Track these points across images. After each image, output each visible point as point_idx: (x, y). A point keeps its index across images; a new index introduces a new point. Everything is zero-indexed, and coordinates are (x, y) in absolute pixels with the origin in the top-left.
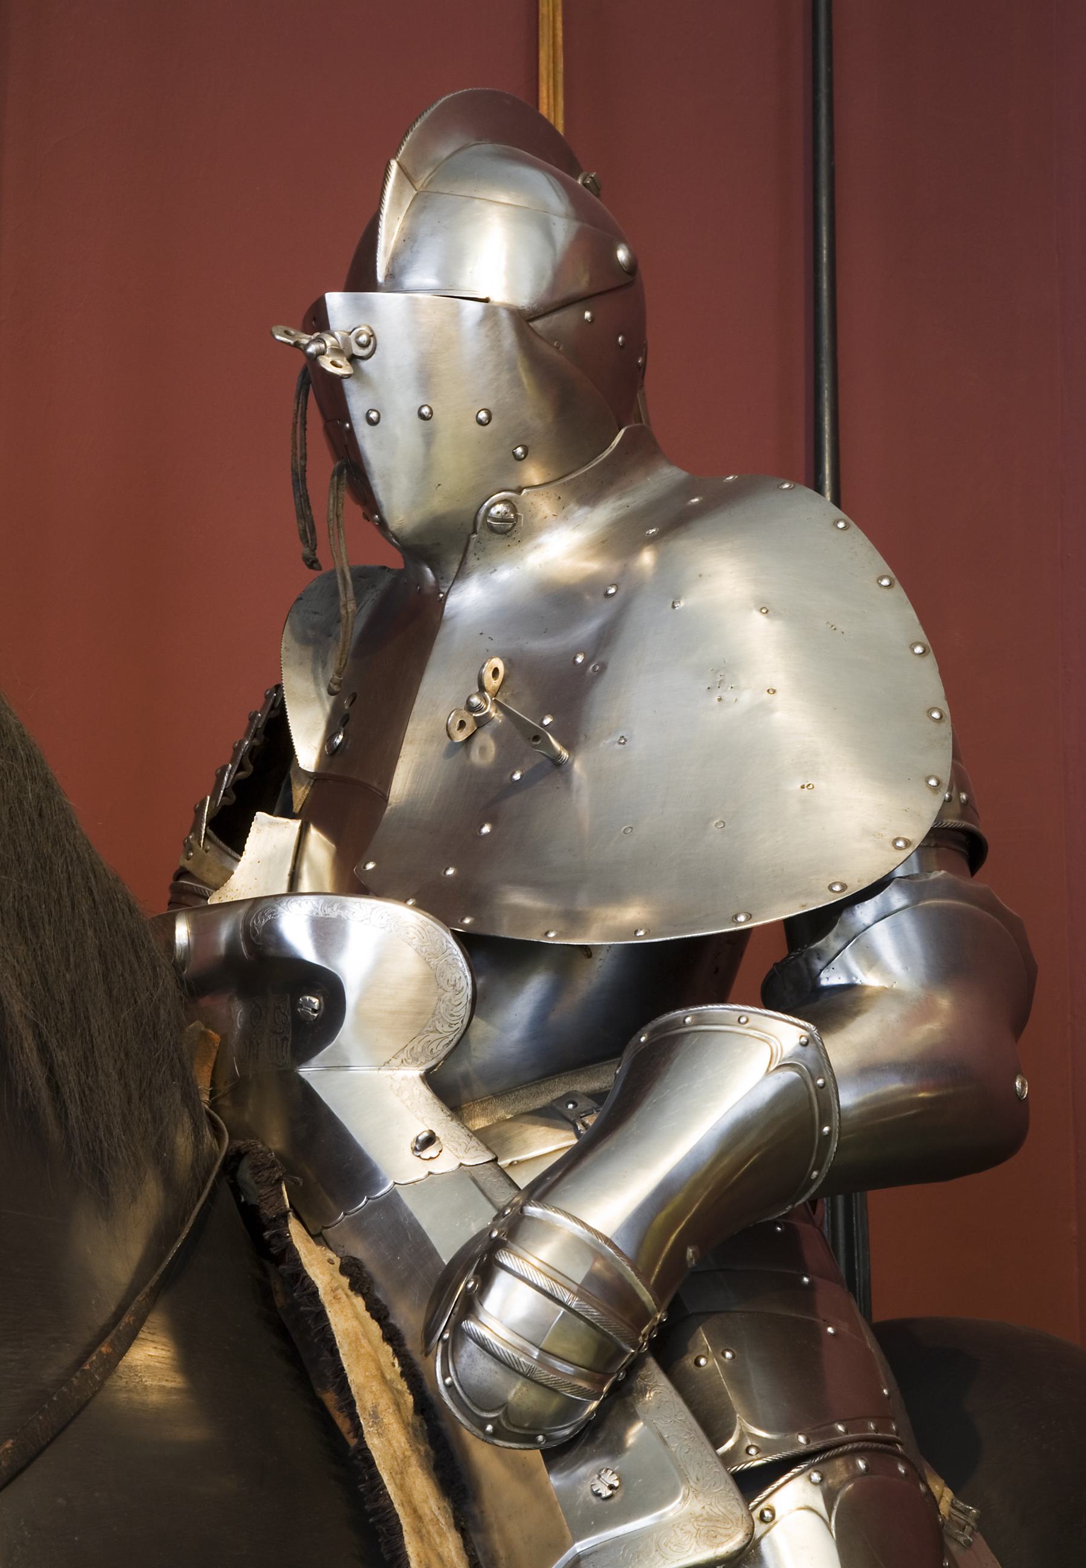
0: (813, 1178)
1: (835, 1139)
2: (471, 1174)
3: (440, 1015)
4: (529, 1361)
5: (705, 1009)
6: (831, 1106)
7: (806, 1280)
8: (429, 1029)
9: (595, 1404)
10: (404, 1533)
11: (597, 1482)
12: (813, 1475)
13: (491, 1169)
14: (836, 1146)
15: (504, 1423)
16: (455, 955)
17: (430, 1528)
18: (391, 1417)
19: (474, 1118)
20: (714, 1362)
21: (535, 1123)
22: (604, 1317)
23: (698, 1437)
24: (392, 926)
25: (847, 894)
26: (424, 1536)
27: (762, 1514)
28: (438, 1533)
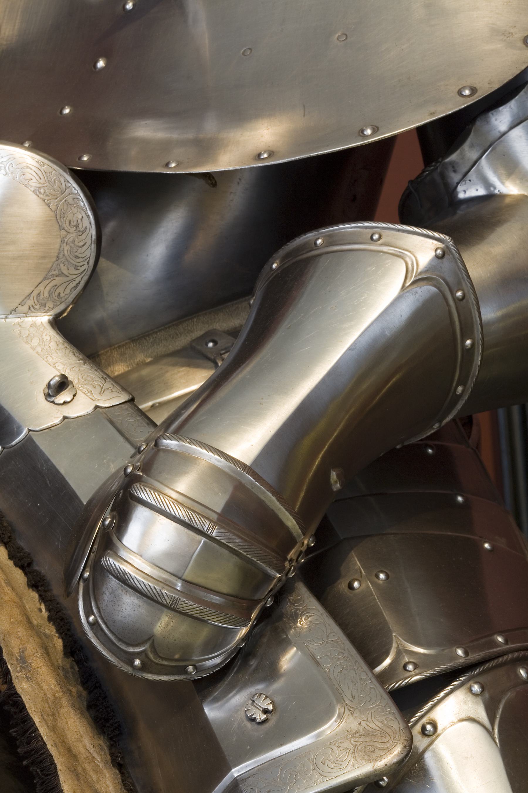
0: (458, 393)
1: (479, 350)
2: (107, 416)
3: (64, 258)
4: (174, 593)
5: (336, 230)
6: (472, 318)
7: (460, 499)
8: (54, 273)
9: (244, 631)
10: (59, 773)
11: (252, 707)
12: (473, 686)
13: (128, 409)
14: (480, 359)
15: (151, 656)
16: (75, 194)
17: (86, 766)
18: (39, 661)
19: (113, 363)
20: (368, 584)
21: (175, 365)
22: (246, 544)
23: (352, 656)
24: (7, 168)
25: (477, 98)
26: (80, 774)
27: (424, 728)
28: (94, 770)
